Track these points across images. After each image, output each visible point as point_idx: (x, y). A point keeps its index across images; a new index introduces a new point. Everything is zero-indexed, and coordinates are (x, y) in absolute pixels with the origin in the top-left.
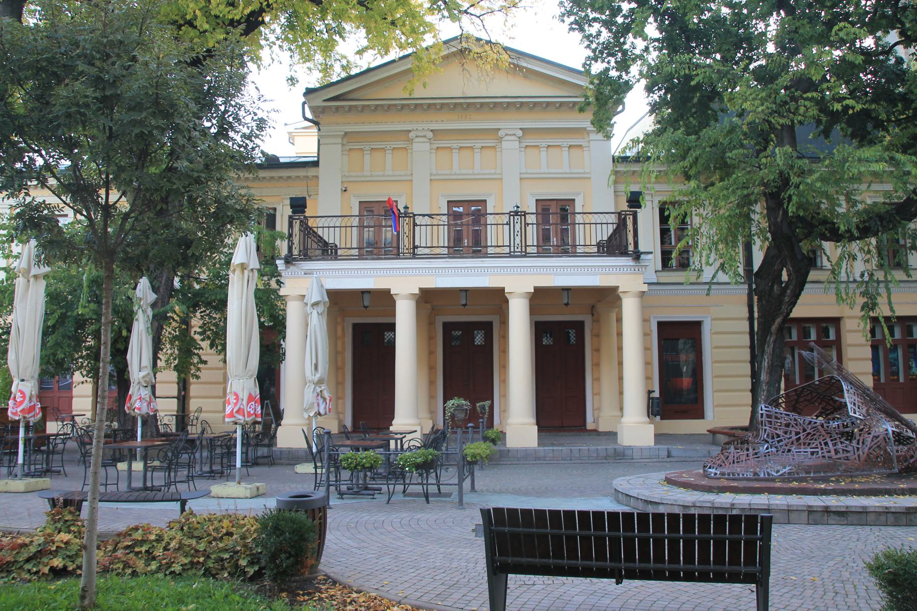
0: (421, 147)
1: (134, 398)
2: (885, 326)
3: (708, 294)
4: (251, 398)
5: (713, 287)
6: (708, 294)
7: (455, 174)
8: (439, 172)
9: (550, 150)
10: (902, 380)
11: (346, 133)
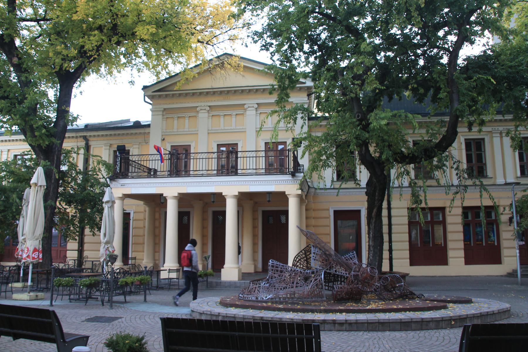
0: (203, 115)
1: (19, 250)
2: (421, 213)
3: (337, 195)
4: (35, 250)
5: (341, 191)
6: (337, 195)
7: (222, 130)
8: (213, 129)
9: (238, 117)
10: (484, 245)
11: (165, 109)
